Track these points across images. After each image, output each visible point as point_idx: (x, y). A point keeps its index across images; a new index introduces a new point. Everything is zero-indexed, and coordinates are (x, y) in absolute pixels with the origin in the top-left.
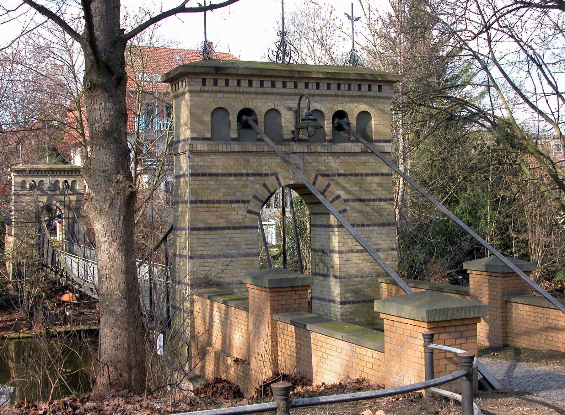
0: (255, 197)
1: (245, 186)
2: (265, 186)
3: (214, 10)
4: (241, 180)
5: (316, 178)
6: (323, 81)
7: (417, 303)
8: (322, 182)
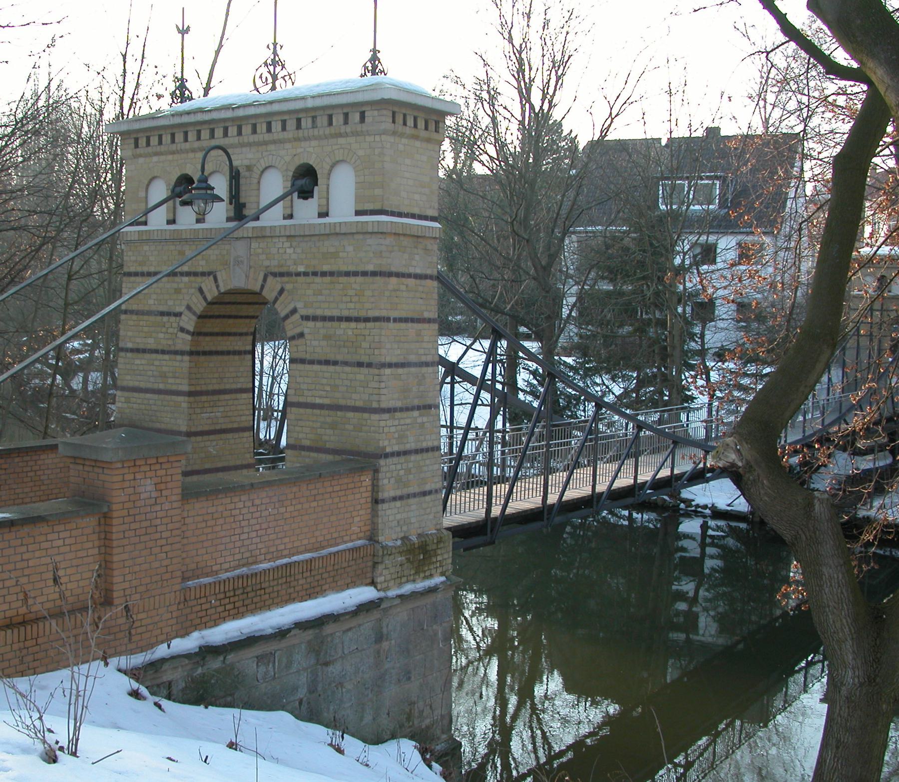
0: (189, 308)
1: (178, 291)
2: (201, 290)
3: (766, 11)
4: (173, 282)
5: (265, 280)
6: (275, 118)
7: (802, 318)
8: (273, 285)
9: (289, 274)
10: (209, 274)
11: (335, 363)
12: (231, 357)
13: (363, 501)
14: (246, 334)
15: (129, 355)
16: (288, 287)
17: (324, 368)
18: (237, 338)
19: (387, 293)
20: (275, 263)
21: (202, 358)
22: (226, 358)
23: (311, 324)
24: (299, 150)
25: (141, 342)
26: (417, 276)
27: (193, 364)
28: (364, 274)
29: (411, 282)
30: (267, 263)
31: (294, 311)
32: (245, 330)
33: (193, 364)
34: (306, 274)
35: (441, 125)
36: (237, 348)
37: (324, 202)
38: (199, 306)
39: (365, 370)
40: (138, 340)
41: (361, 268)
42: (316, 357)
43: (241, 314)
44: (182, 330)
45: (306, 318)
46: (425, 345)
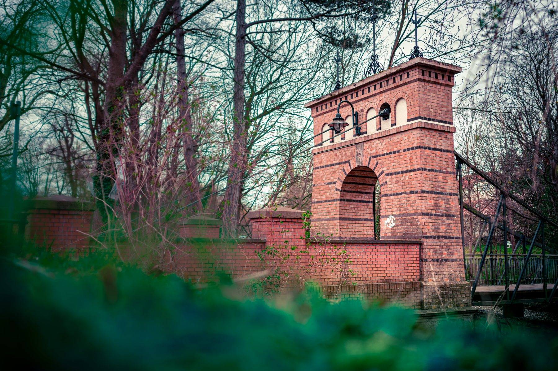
2: (344, 170)
5: (370, 160)
8: (374, 161)
9: (380, 156)
10: (347, 162)
11: (401, 194)
12: (362, 203)
13: (415, 259)
14: (369, 193)
15: (316, 204)
16: (379, 161)
17: (396, 197)
18: (365, 195)
19: (424, 157)
20: (374, 151)
21: (346, 203)
22: (359, 204)
23: (390, 177)
24: (382, 98)
25: (320, 198)
26: (441, 150)
27: (341, 205)
28: (412, 149)
29: (438, 153)
30: (370, 152)
31: (382, 172)
32: (368, 191)
33: (341, 205)
34: (387, 154)
35: (452, 78)
36: (365, 200)
37: (394, 119)
38: (343, 177)
39: (414, 195)
40: (319, 197)
41: (410, 147)
42: (393, 192)
43: (365, 183)
44: (337, 190)
45: (388, 175)
46: (448, 184)
